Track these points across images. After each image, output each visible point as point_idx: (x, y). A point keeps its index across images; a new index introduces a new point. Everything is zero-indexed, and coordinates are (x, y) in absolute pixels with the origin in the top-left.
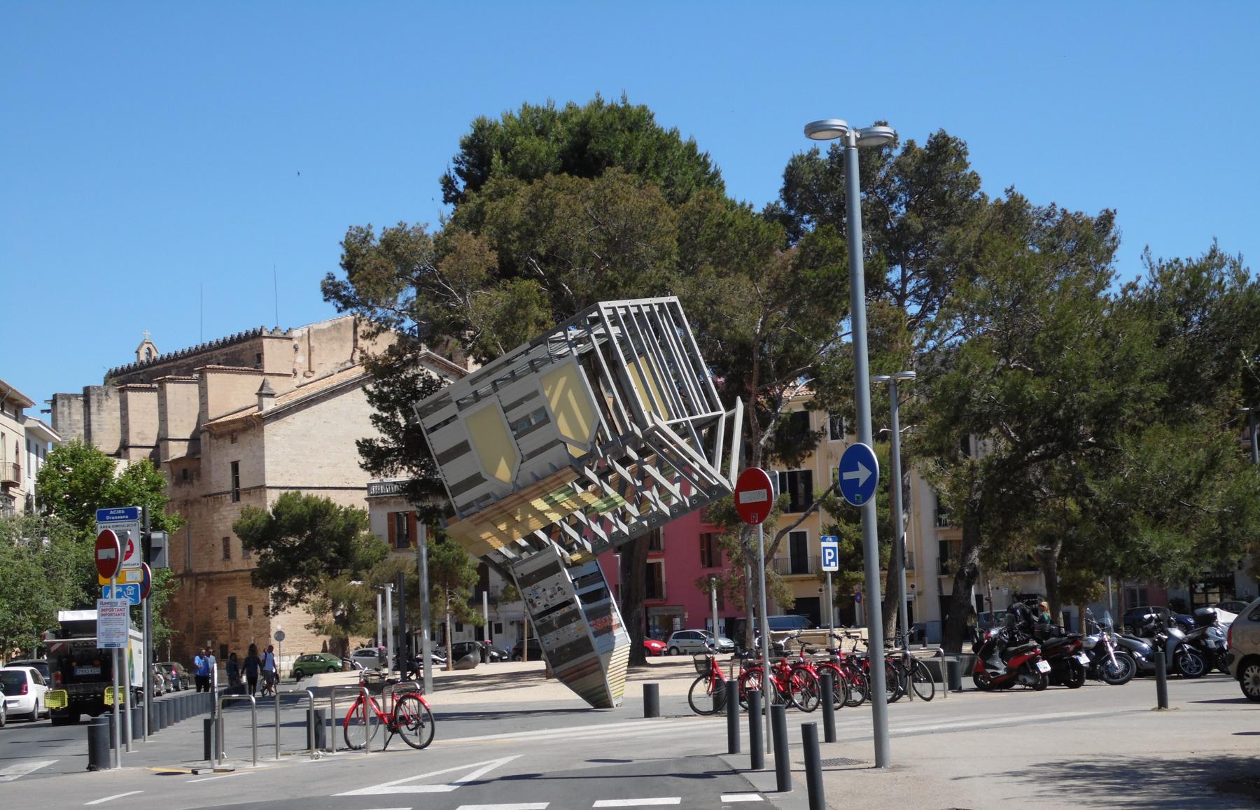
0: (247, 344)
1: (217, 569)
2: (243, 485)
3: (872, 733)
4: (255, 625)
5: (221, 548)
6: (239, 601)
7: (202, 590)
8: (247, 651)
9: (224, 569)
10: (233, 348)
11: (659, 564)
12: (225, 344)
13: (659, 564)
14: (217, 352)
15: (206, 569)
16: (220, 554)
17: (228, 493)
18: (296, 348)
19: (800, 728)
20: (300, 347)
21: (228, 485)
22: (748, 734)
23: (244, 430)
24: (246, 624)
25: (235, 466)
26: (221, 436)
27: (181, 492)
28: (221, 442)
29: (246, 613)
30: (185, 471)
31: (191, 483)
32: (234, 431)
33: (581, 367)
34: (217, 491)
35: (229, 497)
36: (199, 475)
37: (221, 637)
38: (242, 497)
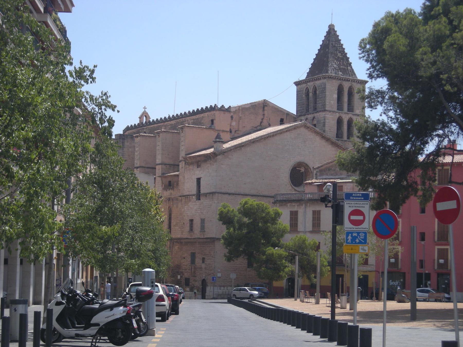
0: (206, 114)
1: (185, 237)
2: (202, 191)
3: (382, 329)
4: (205, 268)
5: (188, 225)
6: (197, 255)
7: (176, 247)
8: (200, 282)
9: (189, 237)
10: (198, 116)
11: (438, 249)
12: (194, 113)
13: (438, 249)
14: (188, 118)
15: (179, 236)
16: (187, 228)
17: (194, 195)
18: (232, 117)
19: (33, 313)
20: (234, 117)
21: (194, 191)
22: (242, 138)
23: (205, 161)
24: (201, 268)
25: (199, 180)
26: (192, 164)
27: (167, 194)
28: (191, 167)
29: (201, 261)
30: (170, 182)
31: (173, 189)
32: (199, 161)
33: (436, 220)
34: (187, 193)
35: (194, 197)
36: (178, 184)
37: (185, 274)
38: (201, 198)
